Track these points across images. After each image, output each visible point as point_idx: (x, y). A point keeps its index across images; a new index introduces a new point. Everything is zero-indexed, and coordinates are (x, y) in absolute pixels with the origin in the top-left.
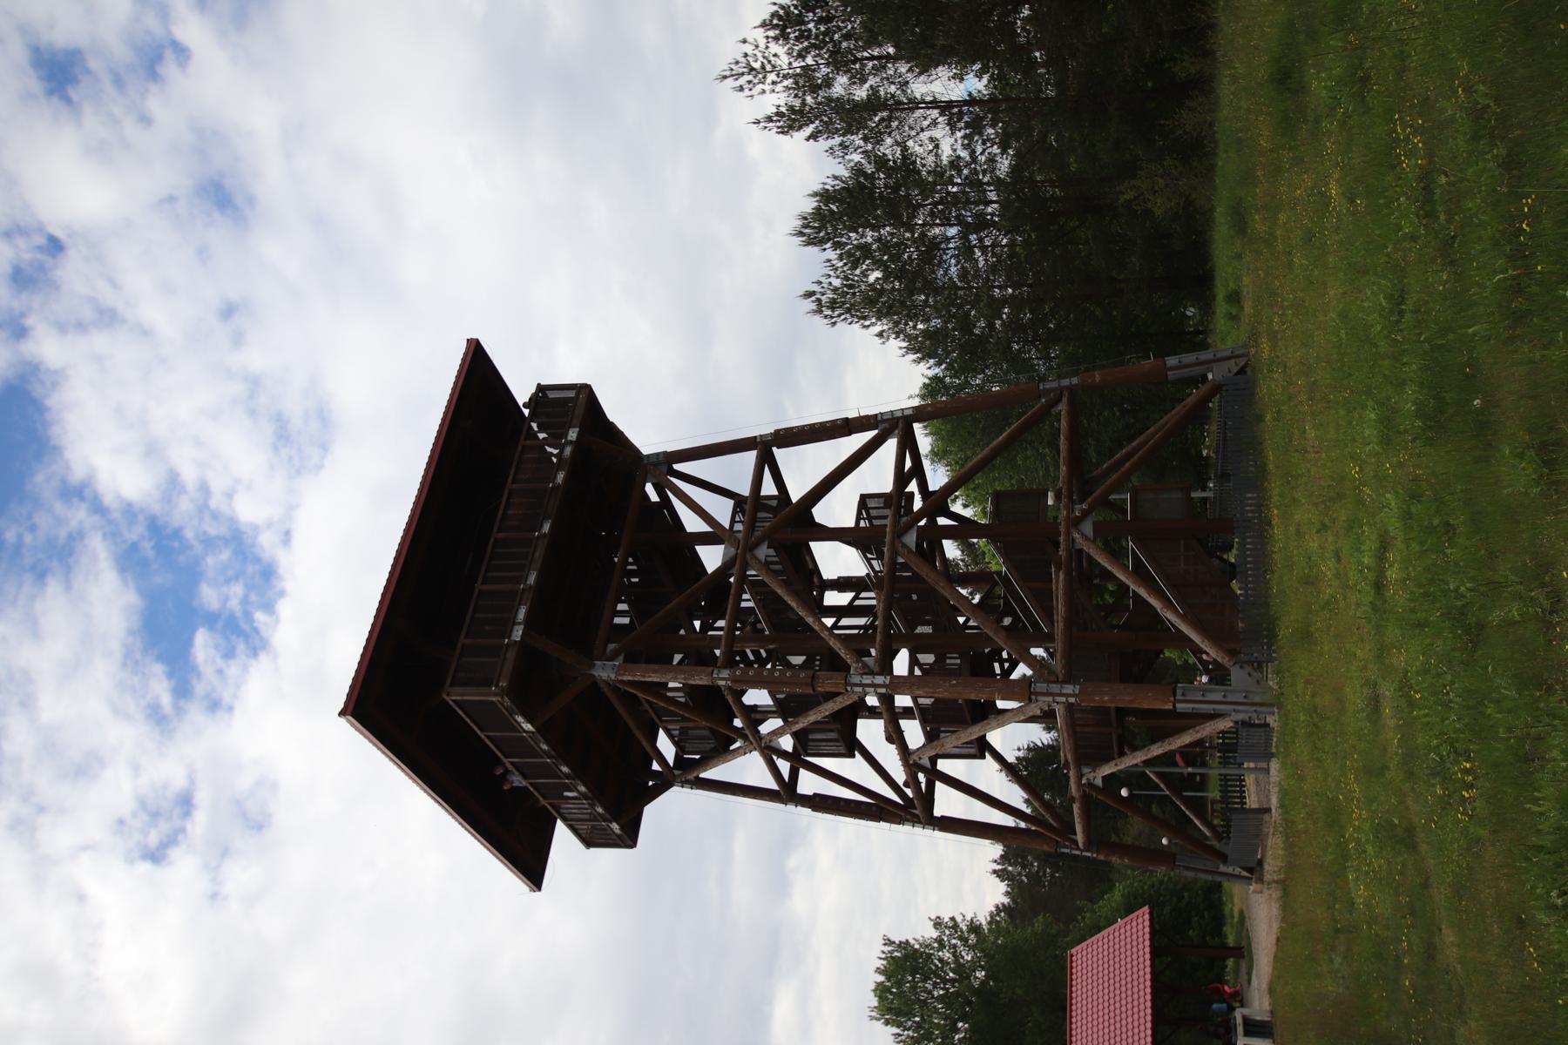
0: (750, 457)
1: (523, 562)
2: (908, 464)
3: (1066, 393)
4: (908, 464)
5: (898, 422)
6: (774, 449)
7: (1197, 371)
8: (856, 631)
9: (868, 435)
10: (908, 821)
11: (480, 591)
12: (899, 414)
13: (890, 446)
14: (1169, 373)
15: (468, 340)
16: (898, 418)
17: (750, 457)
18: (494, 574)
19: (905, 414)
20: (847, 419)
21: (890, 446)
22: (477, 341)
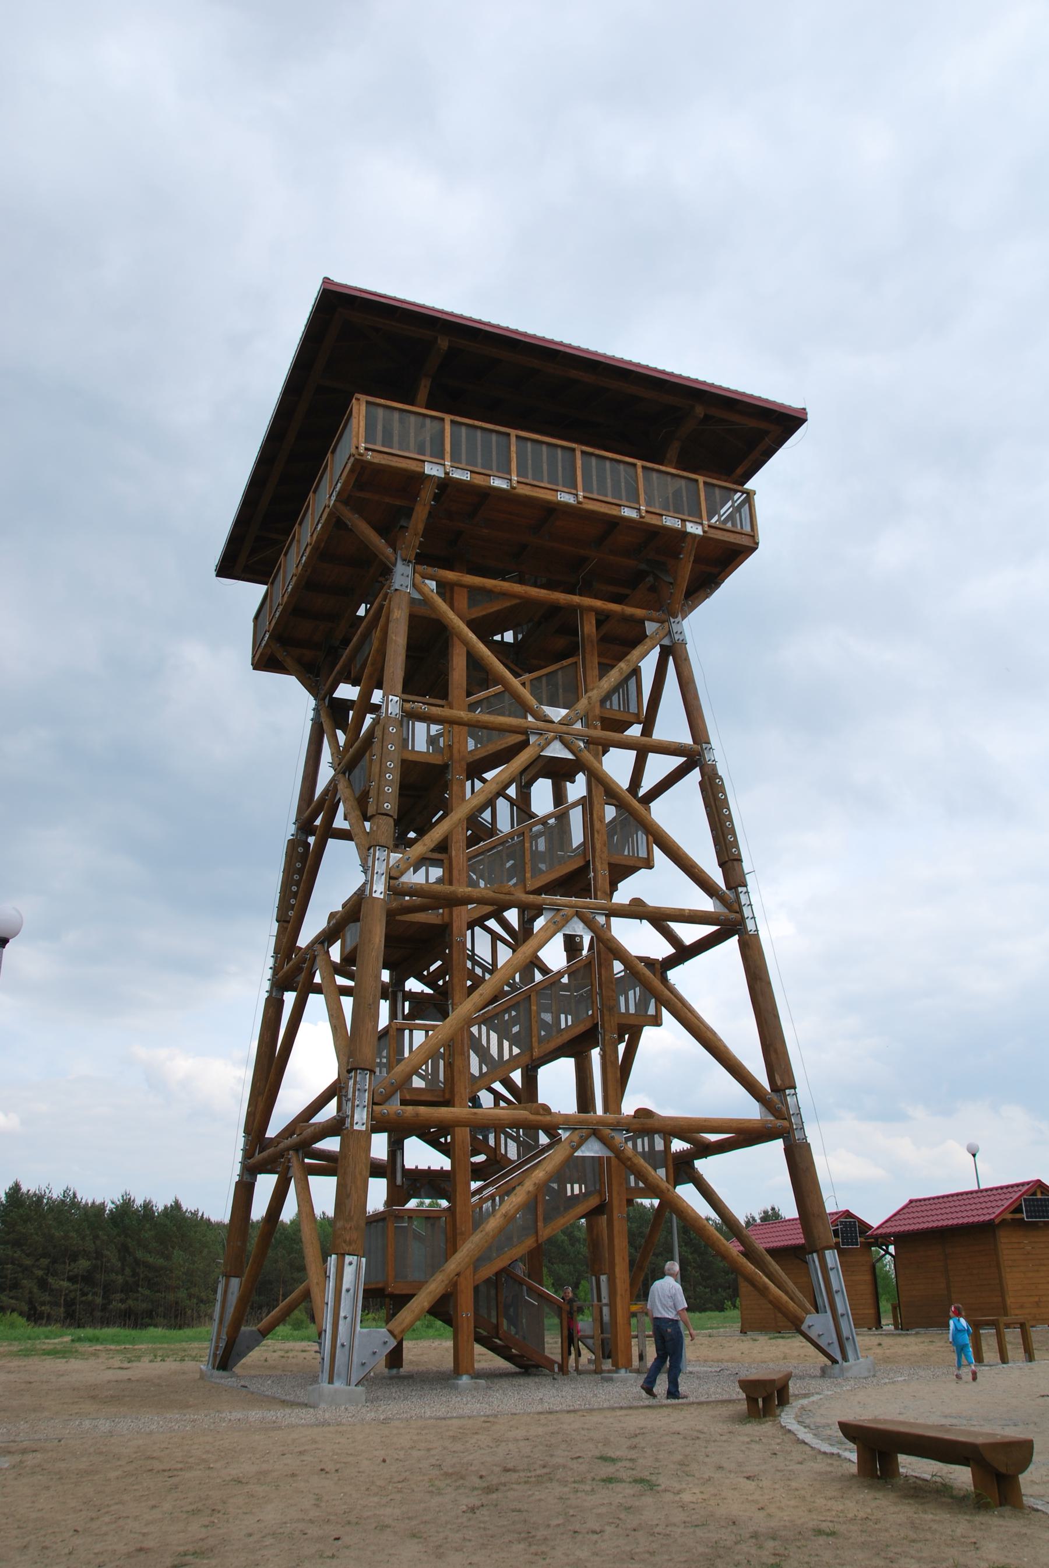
0: (685, 738)
1: (479, 461)
2: (713, 1137)
3: (786, 1123)
4: (713, 1137)
5: (737, 912)
6: (736, 937)
7: (823, 1299)
8: (469, 946)
9: (717, 876)
10: (275, 962)
11: (508, 435)
12: (747, 912)
13: (750, 1110)
14: (815, 1255)
15: (804, 409)
16: (740, 911)
17: (685, 738)
18: (513, 448)
19: (745, 909)
20: (739, 860)
21: (750, 1110)
22: (804, 421)
